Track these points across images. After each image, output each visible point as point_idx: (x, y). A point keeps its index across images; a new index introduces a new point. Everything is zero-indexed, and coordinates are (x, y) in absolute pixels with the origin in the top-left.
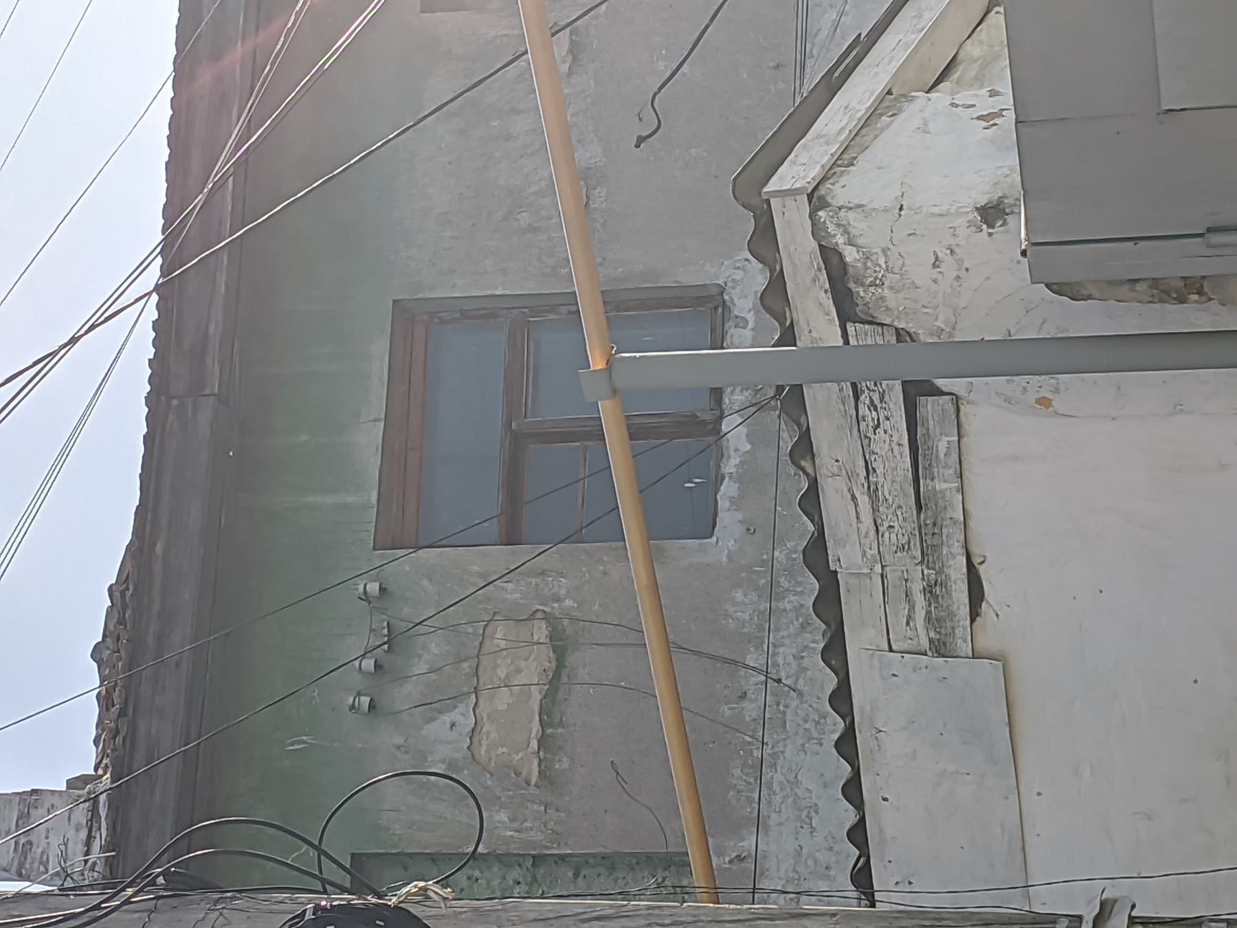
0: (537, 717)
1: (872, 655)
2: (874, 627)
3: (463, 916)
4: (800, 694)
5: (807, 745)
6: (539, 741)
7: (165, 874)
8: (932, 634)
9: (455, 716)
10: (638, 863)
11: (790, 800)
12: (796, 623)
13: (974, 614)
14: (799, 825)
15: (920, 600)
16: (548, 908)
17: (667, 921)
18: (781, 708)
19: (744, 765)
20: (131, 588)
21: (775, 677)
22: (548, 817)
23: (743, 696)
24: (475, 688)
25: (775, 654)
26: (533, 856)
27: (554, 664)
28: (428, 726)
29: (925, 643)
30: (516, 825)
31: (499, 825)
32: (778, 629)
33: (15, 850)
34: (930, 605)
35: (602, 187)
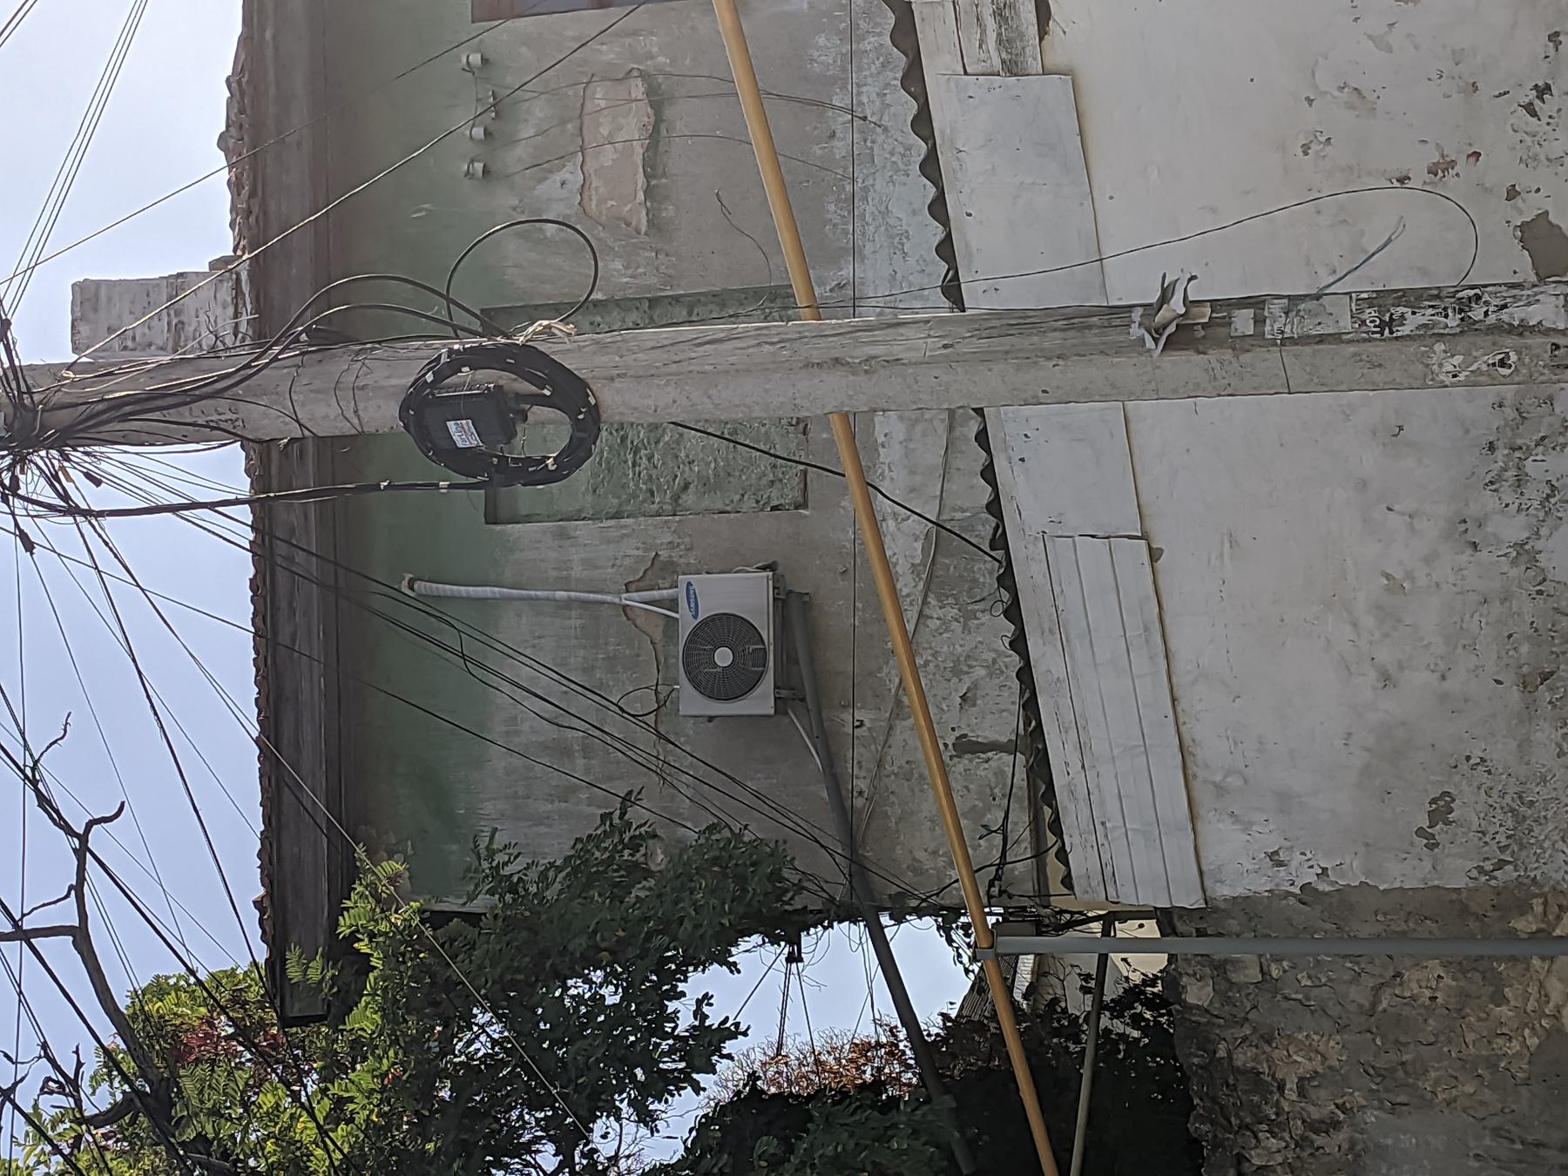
0: (641, 170)
1: (949, 79)
2: (950, 53)
3: (587, 349)
4: (886, 129)
5: (895, 177)
6: (645, 193)
7: (307, 331)
8: (1004, 55)
9: (564, 174)
10: (746, 298)
11: (883, 228)
12: (877, 63)
13: (1042, 33)
14: (892, 251)
15: (991, 23)
16: (665, 336)
17: (775, 340)
18: (869, 144)
19: (838, 200)
20: (246, 75)
21: (861, 115)
22: (659, 262)
23: (833, 135)
24: (581, 147)
25: (859, 94)
26: (650, 300)
27: (653, 119)
28: (540, 186)
29: (997, 65)
30: (630, 272)
31: (615, 273)
32: (860, 69)
33: (169, 330)
34: (1000, 27)
35: (816, 928)
